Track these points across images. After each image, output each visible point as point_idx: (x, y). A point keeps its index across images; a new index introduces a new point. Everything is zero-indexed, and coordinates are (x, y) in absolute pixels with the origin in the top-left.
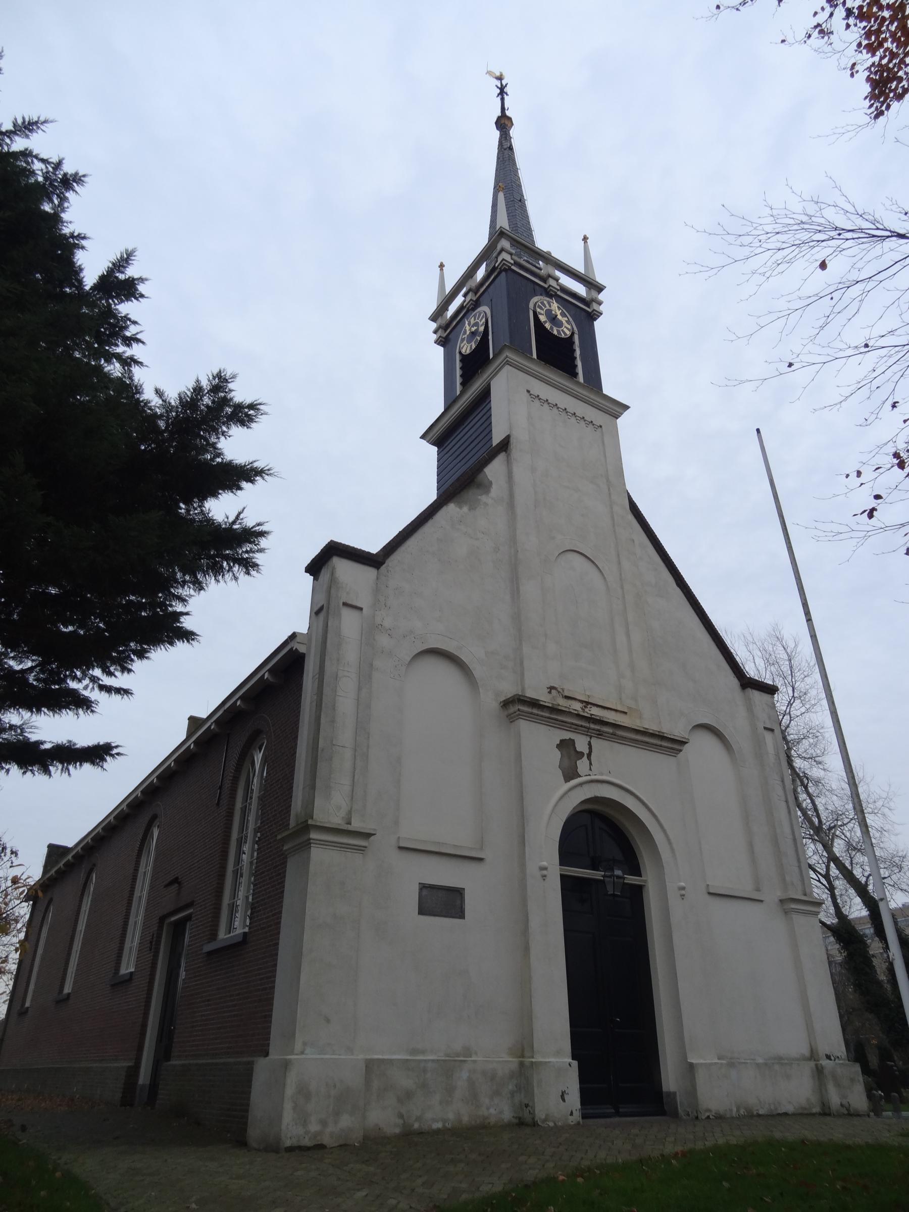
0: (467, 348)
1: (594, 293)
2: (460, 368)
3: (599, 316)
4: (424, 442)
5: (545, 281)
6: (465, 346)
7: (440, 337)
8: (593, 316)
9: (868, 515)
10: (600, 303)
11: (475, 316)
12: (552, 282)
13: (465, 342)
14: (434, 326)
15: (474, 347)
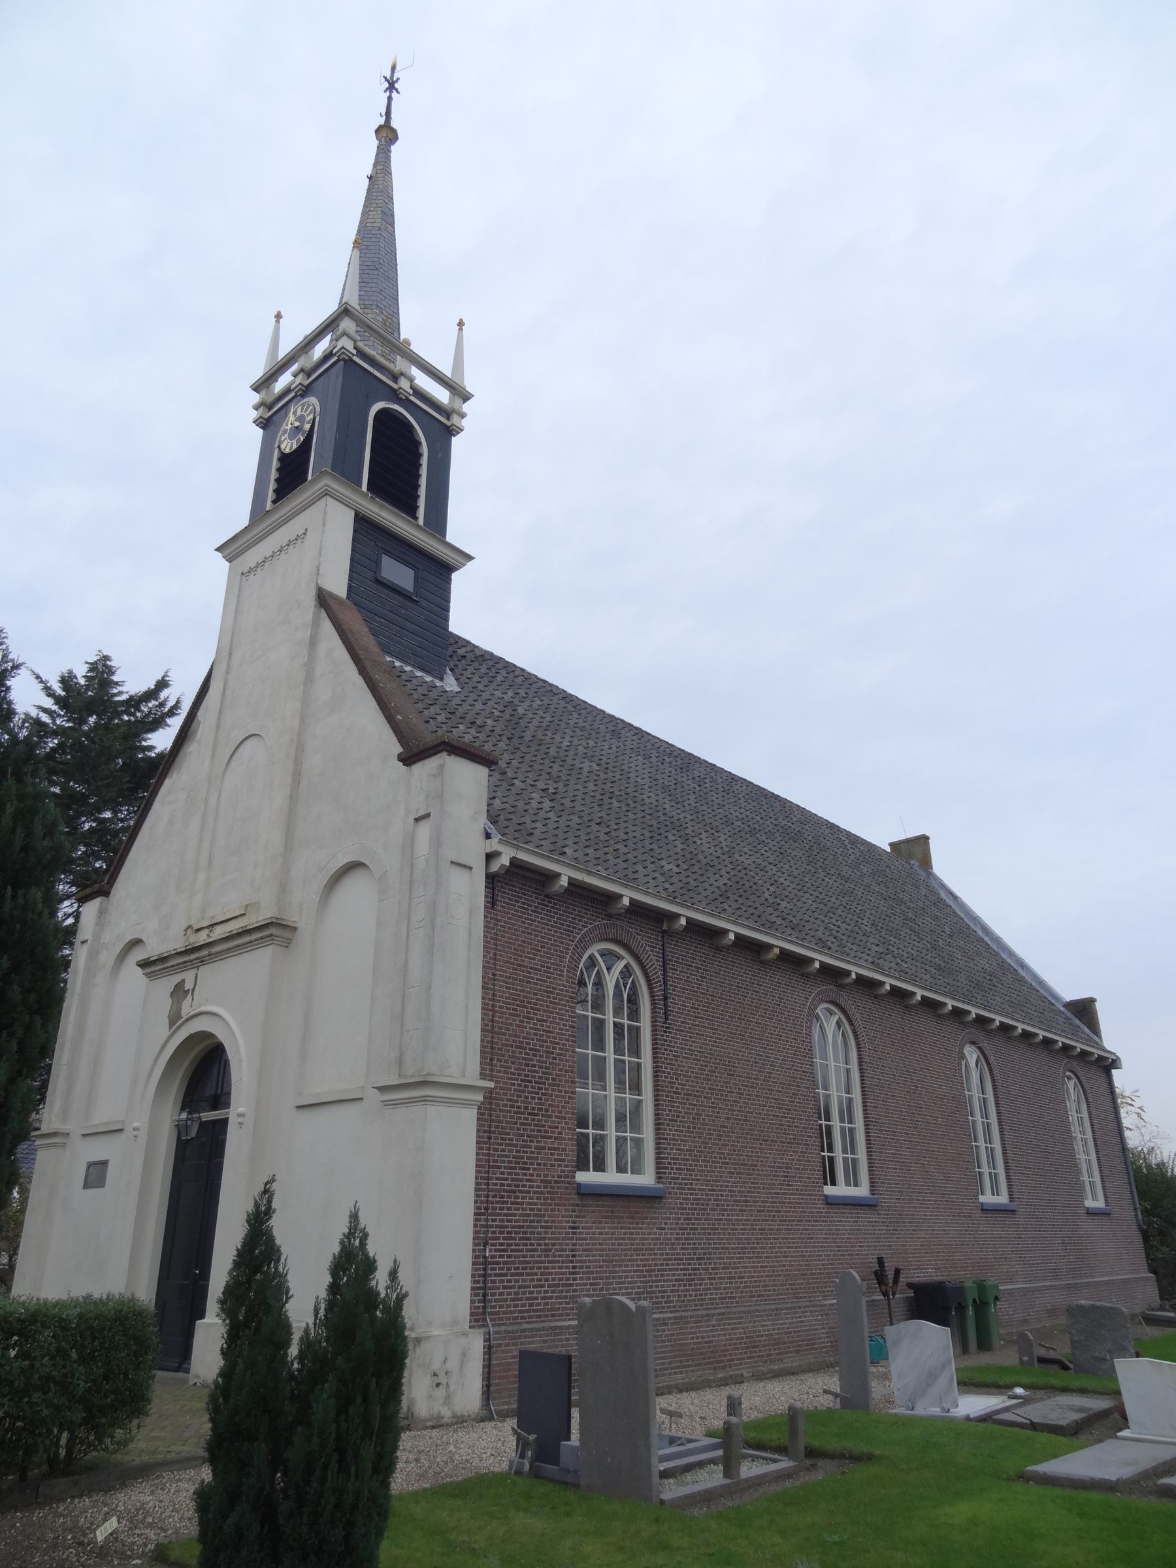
0: (289, 445)
1: (458, 402)
2: (276, 480)
3: (458, 433)
4: (219, 555)
5: (395, 379)
6: (286, 442)
7: (261, 417)
8: (450, 432)
9: (281, 1254)
10: (463, 416)
11: (303, 406)
12: (404, 384)
13: (286, 436)
14: (256, 398)
15: (295, 447)
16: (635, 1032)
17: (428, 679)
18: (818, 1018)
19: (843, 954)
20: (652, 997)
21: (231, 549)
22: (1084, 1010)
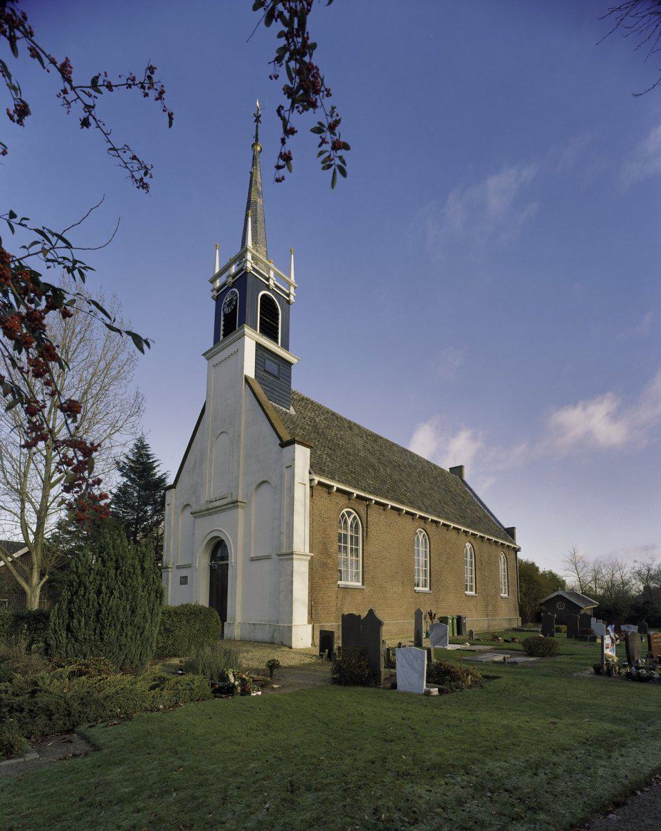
0: (228, 310)
14: (211, 286)
16: (357, 550)
17: (284, 409)
18: (417, 534)
19: (427, 512)
20: (363, 527)
21: (208, 355)
22: (510, 532)
